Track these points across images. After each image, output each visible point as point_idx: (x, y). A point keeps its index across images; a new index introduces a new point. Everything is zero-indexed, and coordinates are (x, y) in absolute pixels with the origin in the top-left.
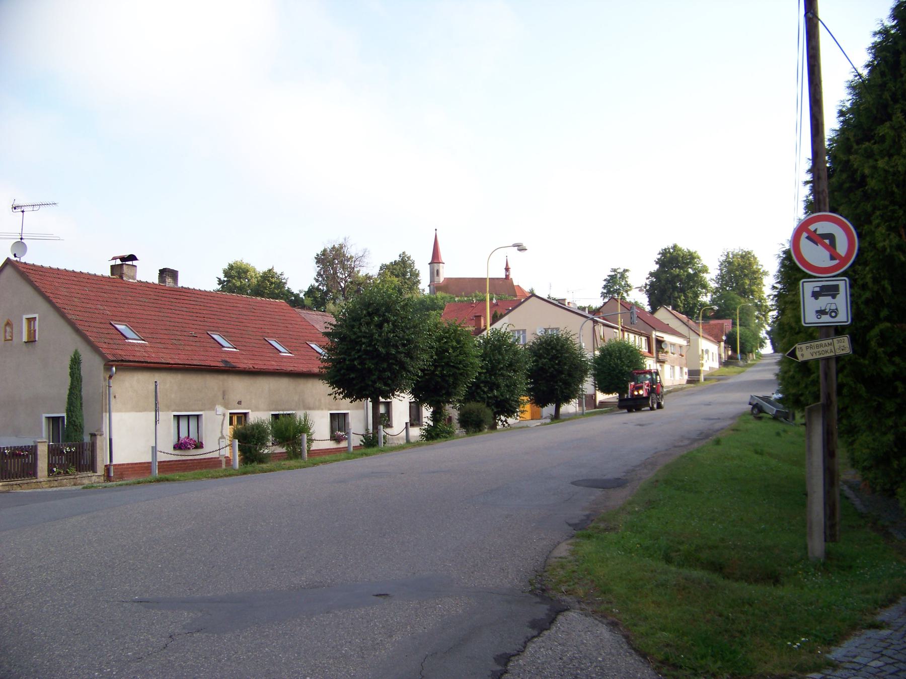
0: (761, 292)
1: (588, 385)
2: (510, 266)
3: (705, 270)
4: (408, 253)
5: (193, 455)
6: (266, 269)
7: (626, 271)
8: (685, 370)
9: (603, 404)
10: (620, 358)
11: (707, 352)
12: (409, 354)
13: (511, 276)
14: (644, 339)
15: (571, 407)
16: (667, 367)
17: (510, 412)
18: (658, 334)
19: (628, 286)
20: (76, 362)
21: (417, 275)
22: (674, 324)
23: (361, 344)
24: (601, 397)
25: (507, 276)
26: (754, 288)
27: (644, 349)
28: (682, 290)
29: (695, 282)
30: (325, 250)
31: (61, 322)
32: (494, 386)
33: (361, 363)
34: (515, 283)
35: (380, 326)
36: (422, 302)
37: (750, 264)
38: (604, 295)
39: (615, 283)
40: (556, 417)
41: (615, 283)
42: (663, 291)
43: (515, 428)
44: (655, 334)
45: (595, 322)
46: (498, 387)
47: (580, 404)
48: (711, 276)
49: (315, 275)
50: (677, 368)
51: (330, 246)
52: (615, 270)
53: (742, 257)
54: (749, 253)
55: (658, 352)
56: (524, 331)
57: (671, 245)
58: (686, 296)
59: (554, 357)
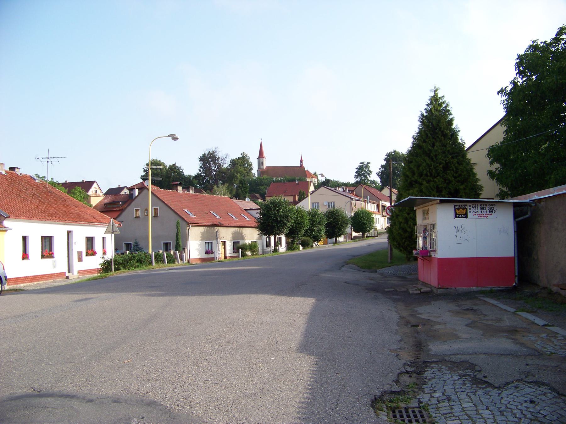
1: (349, 229)
2: (303, 159)
4: (246, 153)
6: (171, 164)
9: (355, 238)
10: (363, 217)
12: (288, 221)
13: (304, 165)
14: (375, 205)
15: (341, 239)
17: (318, 241)
20: (178, 223)
21: (251, 165)
23: (272, 217)
24: (354, 234)
25: (301, 165)
27: (376, 210)
30: (205, 154)
31: (169, 210)
32: (313, 231)
33: (272, 224)
35: (278, 211)
36: (255, 180)
38: (356, 177)
40: (336, 242)
42: (388, 176)
45: (352, 199)
46: (314, 231)
47: (345, 238)
49: (199, 167)
51: (207, 152)
52: (362, 163)
55: (382, 211)
56: (318, 203)
57: (392, 151)
59: (335, 218)
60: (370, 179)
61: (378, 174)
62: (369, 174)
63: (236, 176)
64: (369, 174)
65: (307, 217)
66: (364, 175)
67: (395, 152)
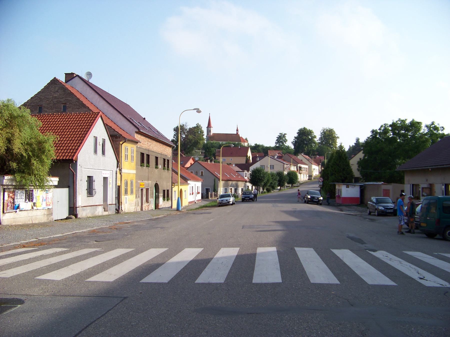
0: (336, 145)
3: (315, 137)
5: (161, 195)
7: (285, 134)
8: (308, 175)
11: (315, 169)
16: (302, 175)
18: (300, 165)
19: (286, 140)
21: (203, 132)
22: (304, 160)
25: (237, 133)
26: (333, 143)
28: (306, 144)
29: (311, 141)
34: (240, 136)
37: (332, 134)
38: (276, 143)
39: (281, 139)
41: (281, 139)
43: (137, 228)
44: (299, 165)
48: (317, 140)
50: (305, 175)
52: (281, 134)
53: (329, 131)
54: (332, 130)
57: (303, 127)
58: (308, 147)
60: (285, 145)
61: (292, 143)
62: (285, 142)
63: (199, 143)
64: (285, 142)
65: (270, 176)
66: (281, 142)
67: (304, 128)
